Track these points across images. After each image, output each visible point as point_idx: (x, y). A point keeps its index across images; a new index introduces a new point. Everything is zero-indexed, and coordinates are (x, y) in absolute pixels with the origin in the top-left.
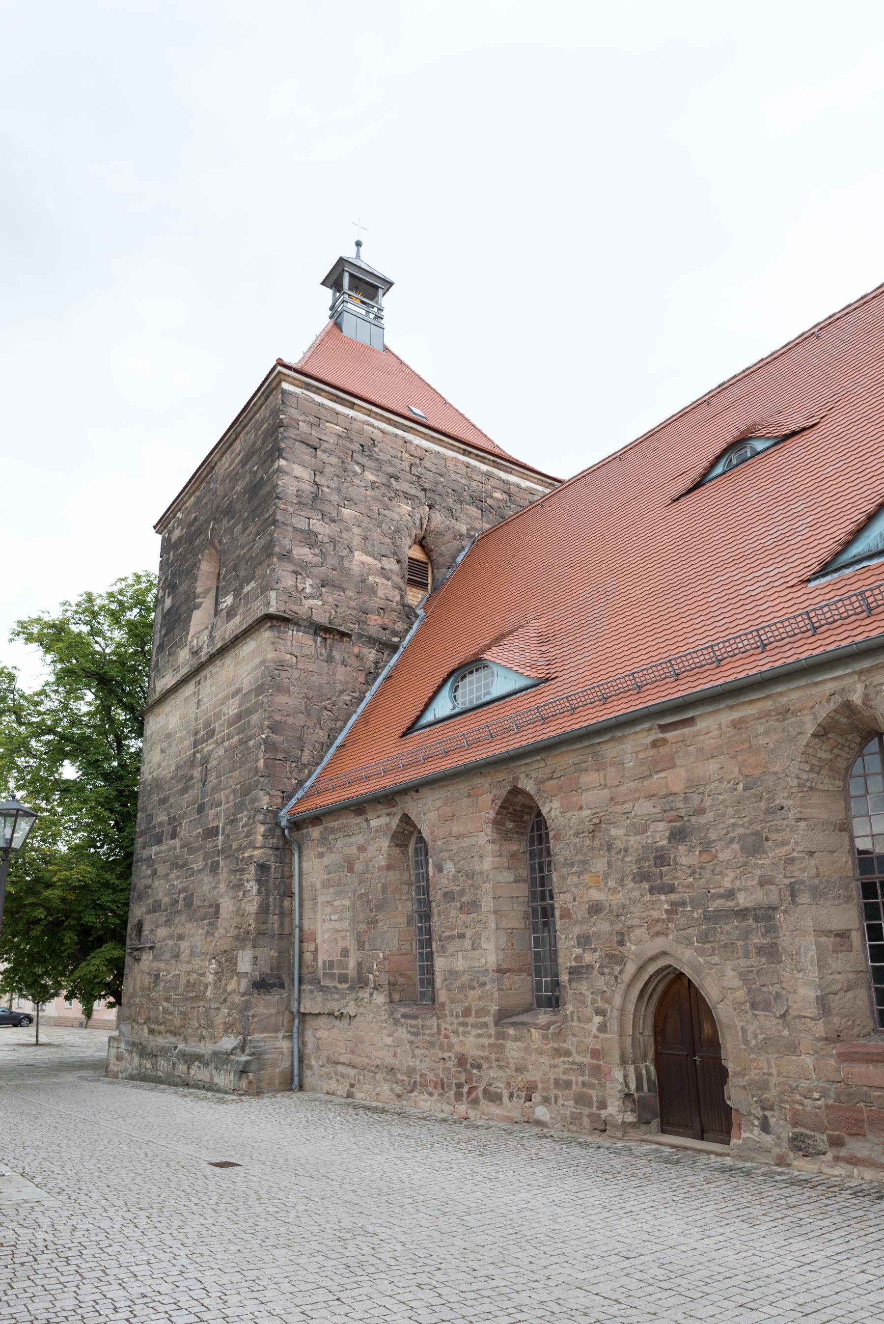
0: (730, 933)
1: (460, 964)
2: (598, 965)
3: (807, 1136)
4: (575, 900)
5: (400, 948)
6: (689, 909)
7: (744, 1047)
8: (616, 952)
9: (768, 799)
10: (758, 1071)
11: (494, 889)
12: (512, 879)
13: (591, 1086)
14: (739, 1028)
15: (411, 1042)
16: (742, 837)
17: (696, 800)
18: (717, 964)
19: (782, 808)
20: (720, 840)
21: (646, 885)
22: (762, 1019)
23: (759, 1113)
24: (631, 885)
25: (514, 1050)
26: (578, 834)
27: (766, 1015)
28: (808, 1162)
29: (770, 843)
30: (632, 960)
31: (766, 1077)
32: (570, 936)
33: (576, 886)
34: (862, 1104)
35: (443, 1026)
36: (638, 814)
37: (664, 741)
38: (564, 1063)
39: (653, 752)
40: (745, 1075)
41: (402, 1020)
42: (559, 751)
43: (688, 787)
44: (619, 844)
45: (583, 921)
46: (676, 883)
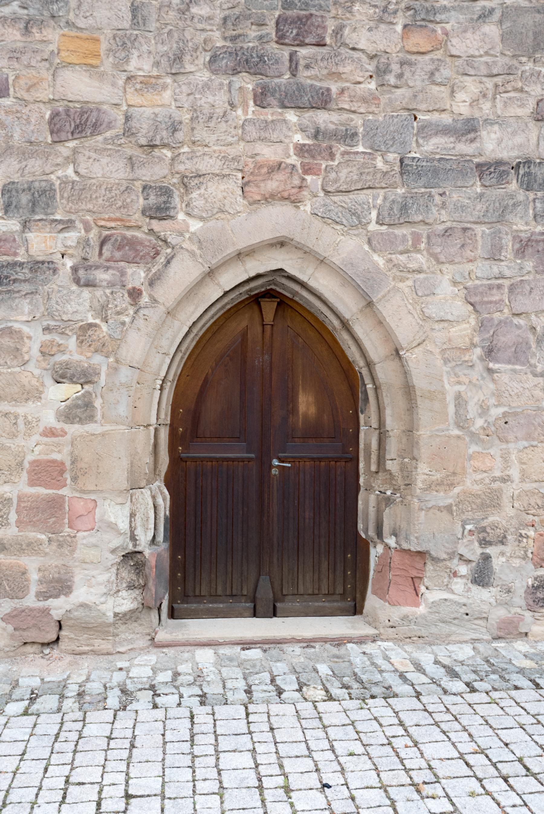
0: (463, 208)
2: (69, 263)
6: (361, 149)
7: (456, 432)
8: (138, 234)
10: (478, 477)
14: (450, 398)
24: (204, 76)
27: (514, 371)
30: (192, 254)
31: (496, 485)
40: (452, 485)
46: (334, 89)
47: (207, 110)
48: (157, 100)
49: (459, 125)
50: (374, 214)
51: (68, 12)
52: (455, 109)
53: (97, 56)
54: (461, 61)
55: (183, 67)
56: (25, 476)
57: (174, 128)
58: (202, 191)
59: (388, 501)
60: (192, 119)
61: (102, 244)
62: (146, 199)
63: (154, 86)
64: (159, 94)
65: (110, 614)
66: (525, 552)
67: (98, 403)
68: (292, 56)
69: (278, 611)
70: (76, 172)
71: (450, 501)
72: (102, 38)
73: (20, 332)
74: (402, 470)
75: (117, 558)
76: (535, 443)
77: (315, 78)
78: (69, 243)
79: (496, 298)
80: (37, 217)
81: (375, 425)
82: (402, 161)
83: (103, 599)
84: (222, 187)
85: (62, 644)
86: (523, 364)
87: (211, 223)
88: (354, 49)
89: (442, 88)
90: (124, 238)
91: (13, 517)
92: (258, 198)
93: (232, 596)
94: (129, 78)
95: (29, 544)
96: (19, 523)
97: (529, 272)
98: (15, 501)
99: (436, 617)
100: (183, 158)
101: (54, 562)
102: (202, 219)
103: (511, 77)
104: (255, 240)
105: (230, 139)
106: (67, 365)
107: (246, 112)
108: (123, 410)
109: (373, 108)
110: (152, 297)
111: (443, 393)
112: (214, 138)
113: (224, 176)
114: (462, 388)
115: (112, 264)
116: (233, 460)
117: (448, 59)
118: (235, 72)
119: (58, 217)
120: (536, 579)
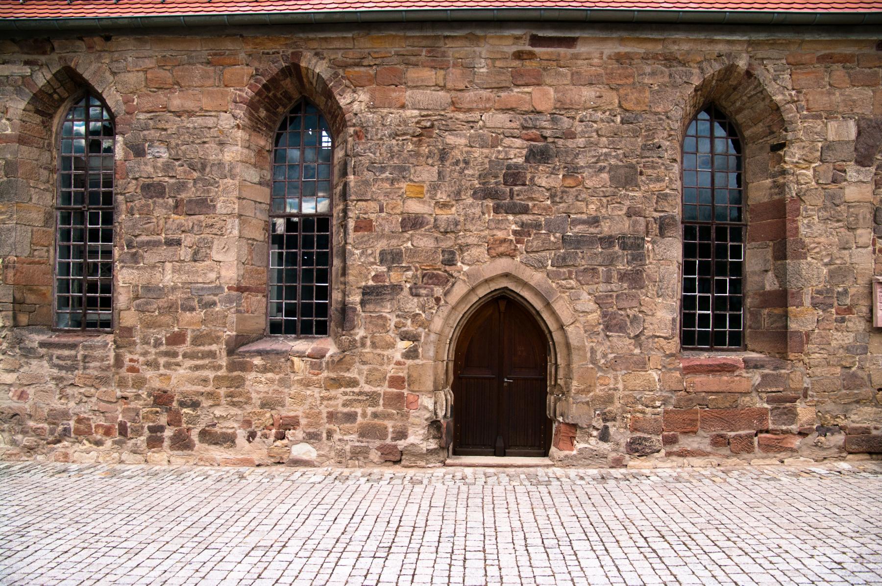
1: (168, 277)
2: (408, 285)
3: (645, 439)
4: (381, 210)
5: (31, 255)
6: (544, 232)
7: (591, 366)
9: (647, 136)
10: (603, 388)
11: (241, 187)
12: (257, 180)
13: (389, 416)
14: (588, 349)
15: (58, 380)
16: (612, 168)
17: (565, 123)
18: (572, 288)
19: (660, 147)
20: (589, 167)
21: (491, 203)
22: (615, 340)
23: (600, 424)
24: (470, 201)
25: (261, 382)
26: (397, 135)
27: (620, 336)
28: (642, 461)
29: (643, 178)
30: (464, 281)
31: (610, 392)
32: (369, 251)
33: (387, 195)
34: (698, 407)
35: (128, 357)
36: (488, 125)
37: (532, 55)
38: (345, 394)
39: (516, 63)
40: (589, 392)
41: (43, 351)
42: (385, 33)
43: (556, 108)
44: (457, 154)
45: (393, 234)
46: (530, 204)
48: (449, 212)
50: (550, 262)
53: (422, 193)
58: (469, 252)
59: (560, 399)
60: (465, 220)
61: (423, 277)
62: (443, 256)
64: (450, 209)
65: (425, 449)
66: (626, 425)
67: (420, 350)
68: (511, 190)
70: (412, 245)
71: (588, 399)
72: (425, 185)
73: (385, 317)
74: (565, 384)
75: (426, 423)
81: (553, 362)
82: (563, 237)
84: (478, 250)
85: (403, 463)
87: (473, 267)
88: (539, 186)
91: (381, 402)
93: (484, 445)
94: (436, 203)
96: (384, 405)
97: (625, 289)
100: (460, 237)
102: (468, 265)
105: (482, 228)
106: (406, 332)
107: (489, 216)
108: (431, 353)
110: (445, 301)
111: (584, 347)
112: (475, 228)
114: (594, 344)
116: (485, 378)
118: (485, 198)
119: (404, 265)
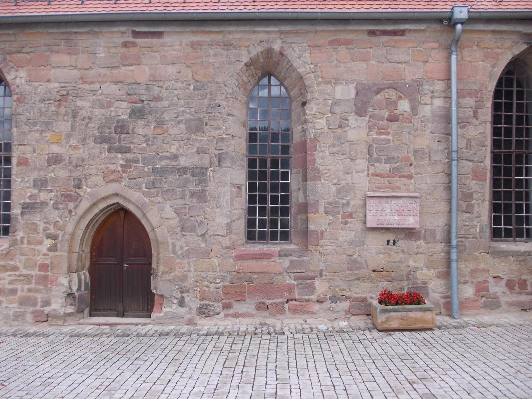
0: (172, 183)
2: (52, 202)
6: (141, 165)
7: (172, 255)
8: (72, 193)
14: (170, 244)
24: (92, 144)
27: (191, 235)
30: (87, 199)
31: (185, 273)
40: (171, 273)
46: (132, 146)
47: (93, 155)
49: (172, 156)
50: (144, 185)
51: (53, 127)
52: (171, 151)
53: (61, 140)
54: (172, 136)
55: (86, 142)
56: (37, 268)
57: (83, 160)
58: (91, 179)
60: (89, 158)
63: (77, 148)
66: (196, 295)
68: (119, 137)
69: (125, 315)
71: (170, 278)
75: (65, 295)
76: (199, 259)
77: (126, 143)
78: (52, 196)
79: (184, 211)
80: (43, 189)
83: (60, 308)
84: (97, 178)
86: (194, 233)
87: (93, 189)
88: (138, 134)
89: (167, 145)
90: (68, 194)
91: (34, 281)
92: (108, 181)
93: (110, 310)
95: (38, 290)
96: (36, 283)
97: (195, 203)
98: (34, 276)
99: (166, 317)
101: (45, 296)
102: (91, 188)
103: (189, 141)
104: (107, 194)
105: (100, 163)
106: (50, 234)
107: (105, 155)
109: (144, 152)
111: (168, 242)
112: (95, 163)
113: (98, 175)
115: (64, 202)
116: (111, 264)
117: (169, 136)
118: (102, 143)
119: (49, 188)
120: (200, 305)
